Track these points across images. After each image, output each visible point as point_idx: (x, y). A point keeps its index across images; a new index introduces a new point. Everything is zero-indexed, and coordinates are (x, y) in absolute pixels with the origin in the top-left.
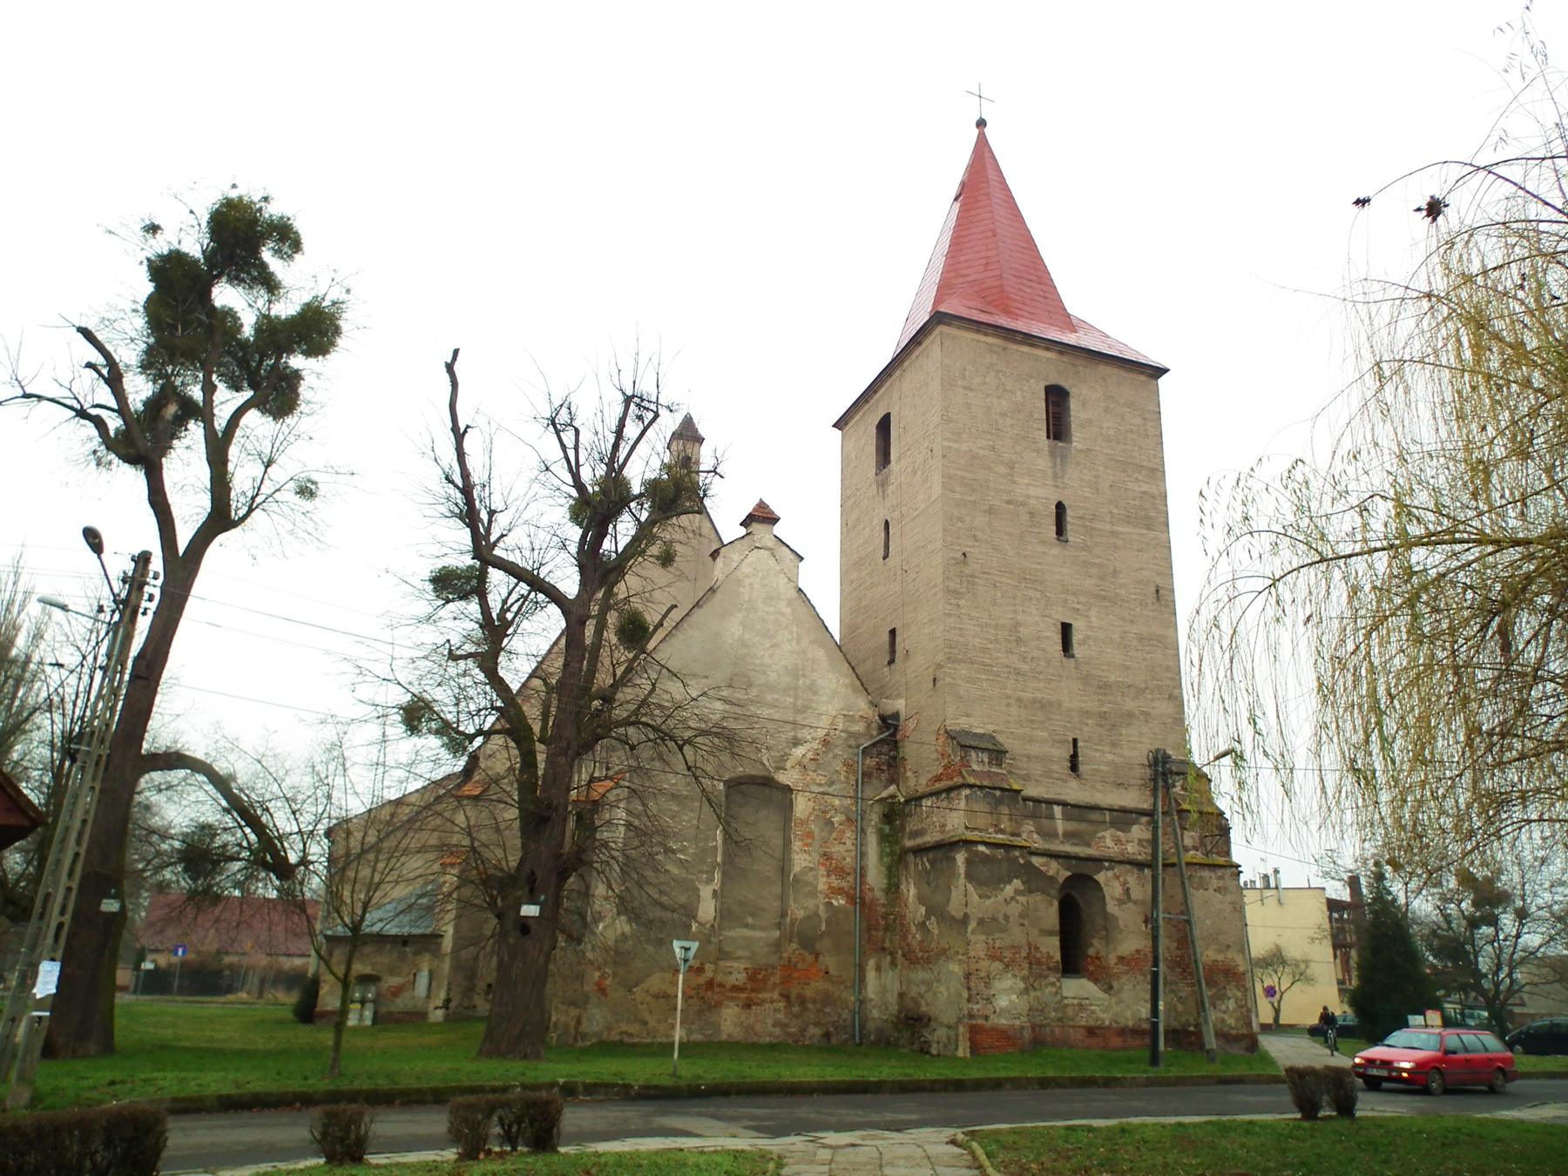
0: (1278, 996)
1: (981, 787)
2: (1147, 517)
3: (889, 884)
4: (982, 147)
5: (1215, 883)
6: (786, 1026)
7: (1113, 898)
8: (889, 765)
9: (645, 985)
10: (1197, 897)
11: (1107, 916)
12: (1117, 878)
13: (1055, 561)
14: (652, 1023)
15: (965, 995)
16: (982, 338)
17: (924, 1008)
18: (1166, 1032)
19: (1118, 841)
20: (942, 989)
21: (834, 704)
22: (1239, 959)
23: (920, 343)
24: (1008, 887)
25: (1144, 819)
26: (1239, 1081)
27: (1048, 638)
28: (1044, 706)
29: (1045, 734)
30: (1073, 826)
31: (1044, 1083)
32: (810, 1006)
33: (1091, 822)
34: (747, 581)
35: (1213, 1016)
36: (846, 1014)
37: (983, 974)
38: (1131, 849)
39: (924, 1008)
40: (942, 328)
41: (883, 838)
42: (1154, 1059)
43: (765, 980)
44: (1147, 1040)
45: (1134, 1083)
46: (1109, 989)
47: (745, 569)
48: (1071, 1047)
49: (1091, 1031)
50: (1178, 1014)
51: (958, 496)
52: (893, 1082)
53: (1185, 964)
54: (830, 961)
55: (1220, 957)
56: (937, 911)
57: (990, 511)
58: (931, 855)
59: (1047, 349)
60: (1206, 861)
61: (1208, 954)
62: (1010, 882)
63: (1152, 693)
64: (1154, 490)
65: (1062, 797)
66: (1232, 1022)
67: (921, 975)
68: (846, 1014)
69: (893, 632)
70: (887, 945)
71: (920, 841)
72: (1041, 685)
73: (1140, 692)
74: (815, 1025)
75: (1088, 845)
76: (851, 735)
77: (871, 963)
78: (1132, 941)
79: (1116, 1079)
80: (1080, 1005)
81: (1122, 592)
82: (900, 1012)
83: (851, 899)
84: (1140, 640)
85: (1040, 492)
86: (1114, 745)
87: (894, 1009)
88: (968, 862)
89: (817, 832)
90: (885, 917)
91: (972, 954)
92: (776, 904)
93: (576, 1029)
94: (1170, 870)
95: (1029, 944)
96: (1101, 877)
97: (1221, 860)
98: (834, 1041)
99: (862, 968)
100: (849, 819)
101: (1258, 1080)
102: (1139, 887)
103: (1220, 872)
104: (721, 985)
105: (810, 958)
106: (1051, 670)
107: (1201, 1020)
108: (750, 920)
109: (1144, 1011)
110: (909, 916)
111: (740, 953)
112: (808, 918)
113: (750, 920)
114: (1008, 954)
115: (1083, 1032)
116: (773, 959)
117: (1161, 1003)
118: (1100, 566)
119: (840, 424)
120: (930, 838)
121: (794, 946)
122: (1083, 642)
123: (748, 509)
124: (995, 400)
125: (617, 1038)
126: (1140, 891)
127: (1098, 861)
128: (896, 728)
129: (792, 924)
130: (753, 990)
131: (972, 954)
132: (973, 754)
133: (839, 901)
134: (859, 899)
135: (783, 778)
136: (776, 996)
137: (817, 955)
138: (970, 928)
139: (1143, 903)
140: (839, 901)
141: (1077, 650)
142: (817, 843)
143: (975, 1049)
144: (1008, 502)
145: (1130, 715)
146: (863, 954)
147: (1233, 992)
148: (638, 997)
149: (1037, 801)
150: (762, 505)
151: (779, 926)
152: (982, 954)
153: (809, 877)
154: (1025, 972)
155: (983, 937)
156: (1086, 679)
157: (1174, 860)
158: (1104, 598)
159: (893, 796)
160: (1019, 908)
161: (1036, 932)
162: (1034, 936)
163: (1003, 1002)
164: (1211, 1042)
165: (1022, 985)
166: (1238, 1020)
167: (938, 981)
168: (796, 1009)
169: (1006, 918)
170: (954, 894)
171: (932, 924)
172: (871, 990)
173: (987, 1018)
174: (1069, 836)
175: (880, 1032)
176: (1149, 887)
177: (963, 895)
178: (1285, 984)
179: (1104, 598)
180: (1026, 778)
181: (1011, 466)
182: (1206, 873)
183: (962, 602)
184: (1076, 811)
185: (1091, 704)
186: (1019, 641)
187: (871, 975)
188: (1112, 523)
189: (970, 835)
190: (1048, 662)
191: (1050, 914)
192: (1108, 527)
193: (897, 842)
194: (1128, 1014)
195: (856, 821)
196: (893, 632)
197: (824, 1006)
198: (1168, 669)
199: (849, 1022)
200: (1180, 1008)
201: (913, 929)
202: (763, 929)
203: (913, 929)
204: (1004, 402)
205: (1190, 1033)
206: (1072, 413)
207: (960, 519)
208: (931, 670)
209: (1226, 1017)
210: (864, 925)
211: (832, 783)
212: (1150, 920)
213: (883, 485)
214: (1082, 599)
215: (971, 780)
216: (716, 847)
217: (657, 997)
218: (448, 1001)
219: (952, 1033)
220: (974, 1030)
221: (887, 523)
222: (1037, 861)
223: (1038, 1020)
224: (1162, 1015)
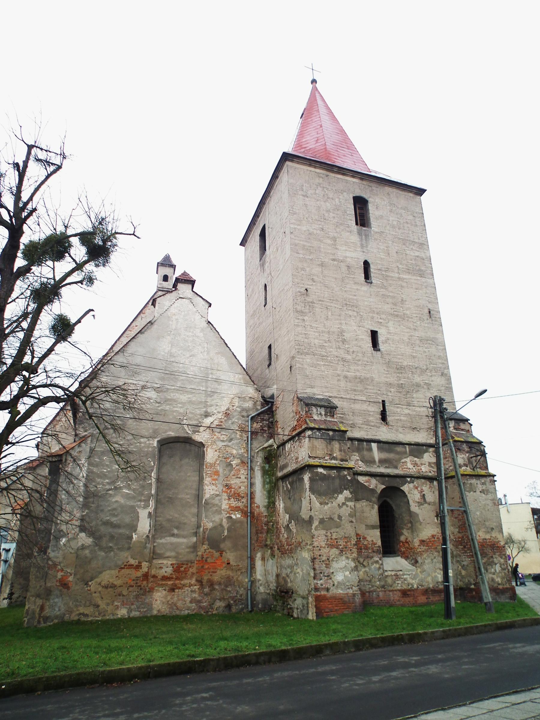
0: (511, 560)
1: (319, 429)
2: (420, 270)
3: (269, 502)
5: (480, 487)
6: (200, 601)
8: (269, 427)
9: (98, 580)
10: (470, 497)
11: (411, 514)
12: (417, 488)
14: (103, 605)
15: (312, 574)
16: (313, 169)
17: (289, 585)
18: (455, 590)
19: (415, 464)
20: (299, 570)
21: (233, 394)
22: (499, 537)
23: (277, 177)
24: (340, 496)
25: (431, 450)
26: (511, 626)
27: (362, 339)
28: (362, 380)
30: (384, 455)
31: (359, 645)
32: (217, 587)
33: (398, 453)
34: (174, 318)
35: (487, 577)
36: (242, 591)
37: (324, 558)
38: (425, 469)
39: (289, 585)
40: (288, 163)
41: (265, 473)
42: (448, 613)
43: (186, 571)
44: (443, 595)
45: (433, 637)
46: (415, 563)
47: (173, 310)
48: (391, 606)
49: (405, 593)
50: (463, 577)
51: (301, 256)
52: (218, 660)
53: (466, 542)
54: (230, 556)
55: (488, 537)
56: (295, 517)
57: (322, 265)
59: (353, 177)
60: (473, 473)
61: (480, 535)
62: (341, 492)
63: (431, 371)
64: (423, 255)
65: (377, 438)
66: (499, 580)
67: (288, 561)
68: (242, 591)
69: (270, 347)
70: (268, 543)
71: (285, 471)
72: (359, 368)
73: (423, 372)
74: (220, 600)
75: (396, 467)
76: (243, 410)
77: (259, 555)
78: (429, 530)
79: (419, 635)
80: (396, 575)
81: (408, 312)
82: (277, 587)
83: (244, 513)
84: (421, 341)
85: (354, 255)
87: (273, 586)
88: (311, 480)
89: (221, 471)
90: (267, 524)
91: (316, 544)
92: (194, 520)
93: (40, 614)
94: (450, 481)
95: (357, 535)
96: (405, 488)
97: (483, 472)
98: (234, 610)
99: (252, 559)
100: (243, 462)
101: (524, 624)
102: (431, 493)
103: (483, 480)
104: (154, 576)
105: (217, 554)
107: (479, 580)
108: (176, 531)
109: (440, 577)
110: (281, 522)
111: (168, 554)
112: (215, 528)
113: (176, 531)
114: (342, 543)
115: (399, 594)
116: (192, 557)
117: (450, 571)
118: (393, 297)
119: (243, 243)
121: (205, 547)
123: (160, 259)
124: (322, 203)
125: (76, 618)
126: (432, 496)
127: (403, 478)
128: (272, 403)
129: (204, 532)
130: (177, 578)
131: (316, 544)
132: (314, 409)
133: (237, 516)
134: (250, 514)
135: (198, 438)
136: (193, 581)
137: (221, 552)
138: (313, 527)
139: (434, 503)
140: (237, 516)
142: (221, 479)
143: (319, 613)
144: (334, 260)
145: (418, 385)
146: (253, 551)
147: (497, 559)
148: (93, 588)
149: (360, 440)
150: (185, 272)
151: (196, 534)
152: (323, 544)
153: (216, 501)
154: (355, 555)
155: (324, 532)
156: (388, 364)
157: (453, 473)
158: (397, 316)
159: (271, 446)
160: (349, 510)
161: (364, 526)
162: (362, 530)
163: (339, 577)
164: (488, 597)
165: (353, 565)
166: (503, 578)
167: (297, 564)
168: (206, 590)
169: (340, 517)
170: (304, 503)
171: (293, 526)
172: (259, 574)
173: (328, 590)
174: (382, 462)
175: (265, 602)
176: (437, 493)
177: (311, 504)
178: (515, 553)
179: (397, 316)
180: (353, 426)
181: (334, 239)
182: (474, 481)
184: (386, 446)
185: (392, 379)
186: (344, 341)
187: (259, 563)
188: (399, 273)
189: (312, 462)
190: (364, 353)
191: (372, 514)
192: (397, 275)
193: (273, 475)
194: (429, 579)
195: (247, 463)
196: (270, 347)
197: (227, 586)
198: (439, 357)
199: (244, 597)
200: (463, 572)
201: (283, 530)
202: (184, 537)
203: (283, 530)
204: (328, 204)
205: (471, 590)
206: (370, 212)
207: (303, 269)
208: (289, 362)
209: (495, 577)
210: (254, 530)
211: (231, 440)
212: (440, 515)
213: (262, 265)
214: (383, 316)
215: (312, 425)
216: (151, 484)
217: (106, 587)
218: (11, 594)
219: (305, 602)
220: (318, 599)
221: (266, 285)
222: (361, 479)
223: (367, 588)
224: (451, 580)
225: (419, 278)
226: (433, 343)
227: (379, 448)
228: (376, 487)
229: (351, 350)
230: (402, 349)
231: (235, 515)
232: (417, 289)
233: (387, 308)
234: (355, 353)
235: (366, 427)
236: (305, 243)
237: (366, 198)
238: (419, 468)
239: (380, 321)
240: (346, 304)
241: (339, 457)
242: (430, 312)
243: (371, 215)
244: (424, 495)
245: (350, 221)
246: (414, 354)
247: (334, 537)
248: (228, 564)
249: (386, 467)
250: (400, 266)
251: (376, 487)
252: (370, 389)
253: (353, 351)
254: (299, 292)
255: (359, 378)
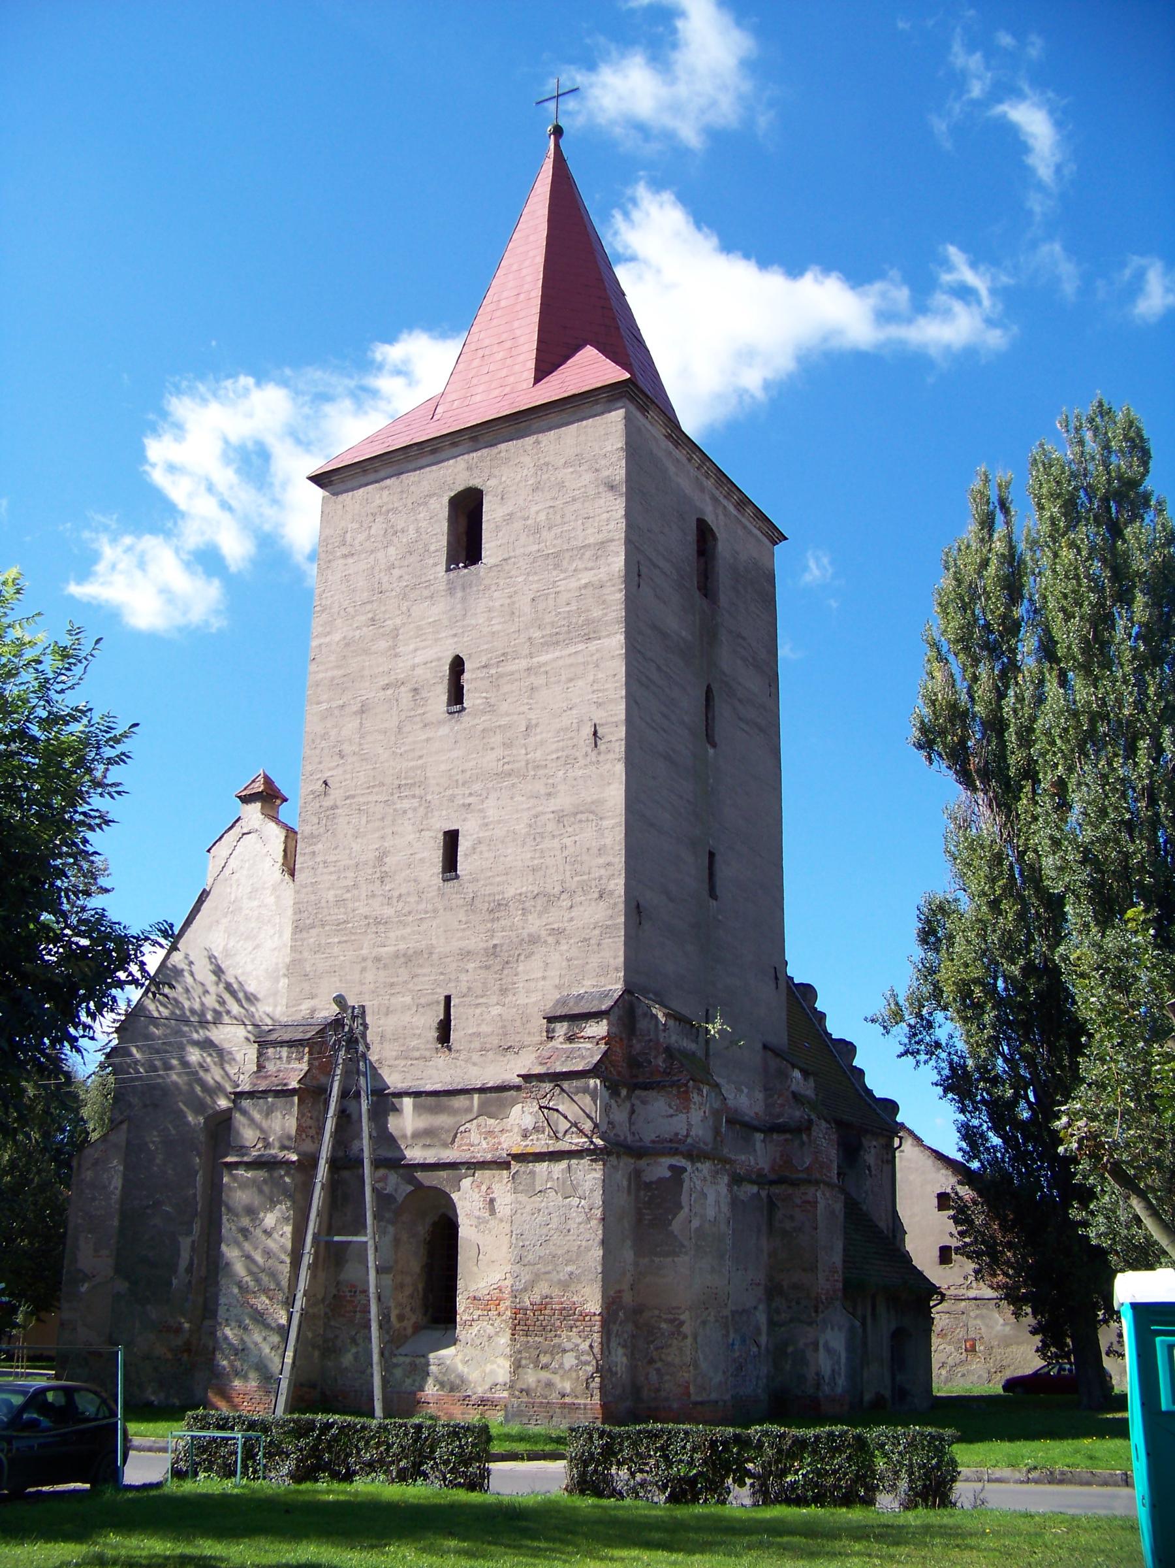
13: (443, 746)
28: (408, 959)
29: (408, 999)
30: (423, 1122)
73: (551, 900)
86: (504, 991)
106: (422, 906)
122: (590, 811)
144: (385, 688)
145: (534, 940)
184: (431, 1100)
225: (581, 647)
226: (591, 817)
227: (416, 1107)
228: (396, 1190)
229: (396, 894)
230: (508, 859)
232: (571, 680)
233: (490, 761)
234: (403, 899)
235: (403, 1063)
236: (721, 498)
238: (496, 1140)
251: (396, 1190)
252: (424, 975)
253: (400, 895)
254: (312, 792)
255: (404, 955)
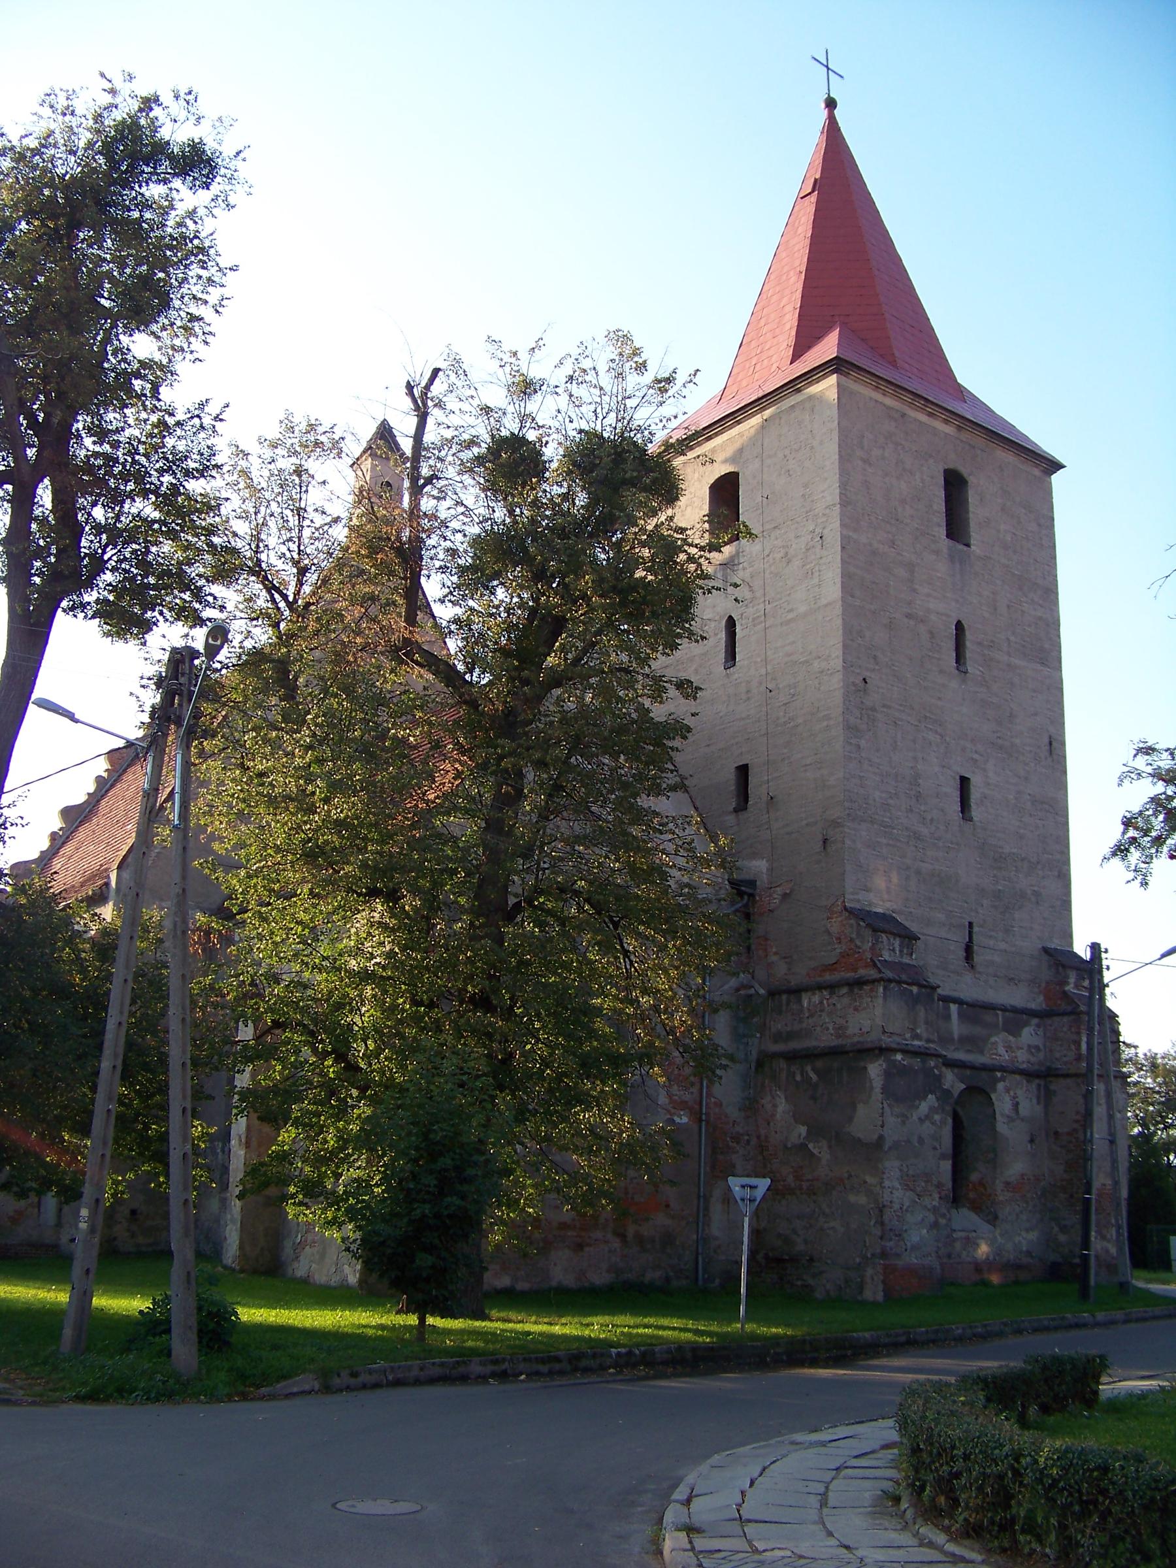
4: (832, 131)
7: (1002, 1115)
17: (801, 1247)
19: (1008, 1048)
58: (819, 1064)
59: (946, 422)
75: (982, 1052)
80: (968, 1238)
81: (1017, 741)
120: (826, 1040)
127: (989, 1069)
128: (751, 895)
133: (683, 1119)
141: (976, 813)
169: (921, 1140)
179: (1001, 748)
183: (863, 743)
186: (918, 796)
188: (1009, 654)
189: (887, 1041)
200: (1062, 1238)
225: (1039, 667)
227: (961, 1015)
231: (680, 1116)
232: (1034, 691)
237: (965, 475)
239: (976, 756)
240: (926, 717)
241: (925, 1035)
242: (1051, 744)
243: (971, 515)
244: (1018, 1103)
245: (936, 529)
246: (1022, 831)
247: (911, 1172)
248: (668, 1206)
249: (969, 1051)
250: (1012, 638)
